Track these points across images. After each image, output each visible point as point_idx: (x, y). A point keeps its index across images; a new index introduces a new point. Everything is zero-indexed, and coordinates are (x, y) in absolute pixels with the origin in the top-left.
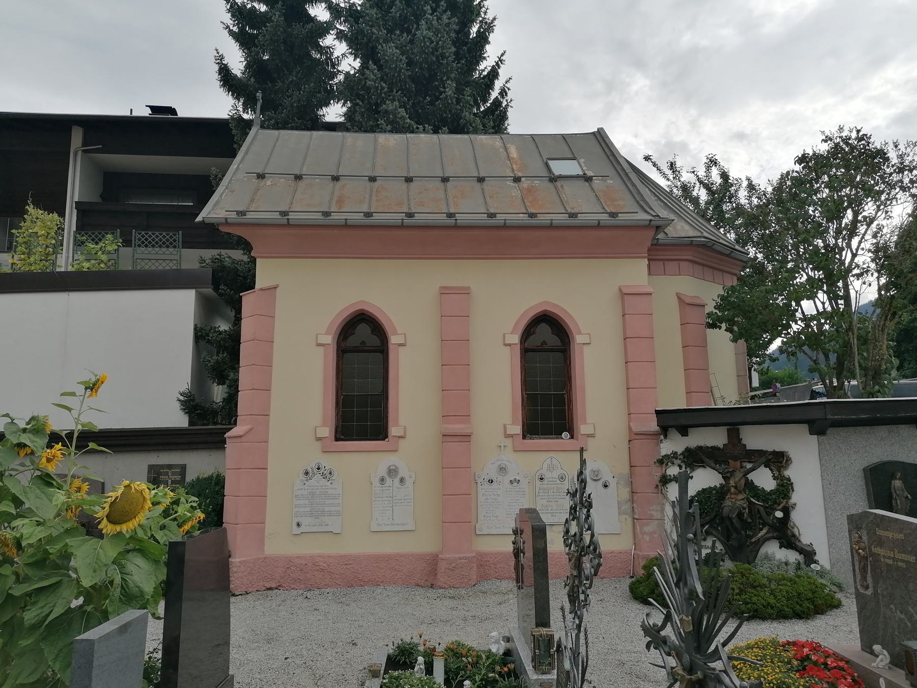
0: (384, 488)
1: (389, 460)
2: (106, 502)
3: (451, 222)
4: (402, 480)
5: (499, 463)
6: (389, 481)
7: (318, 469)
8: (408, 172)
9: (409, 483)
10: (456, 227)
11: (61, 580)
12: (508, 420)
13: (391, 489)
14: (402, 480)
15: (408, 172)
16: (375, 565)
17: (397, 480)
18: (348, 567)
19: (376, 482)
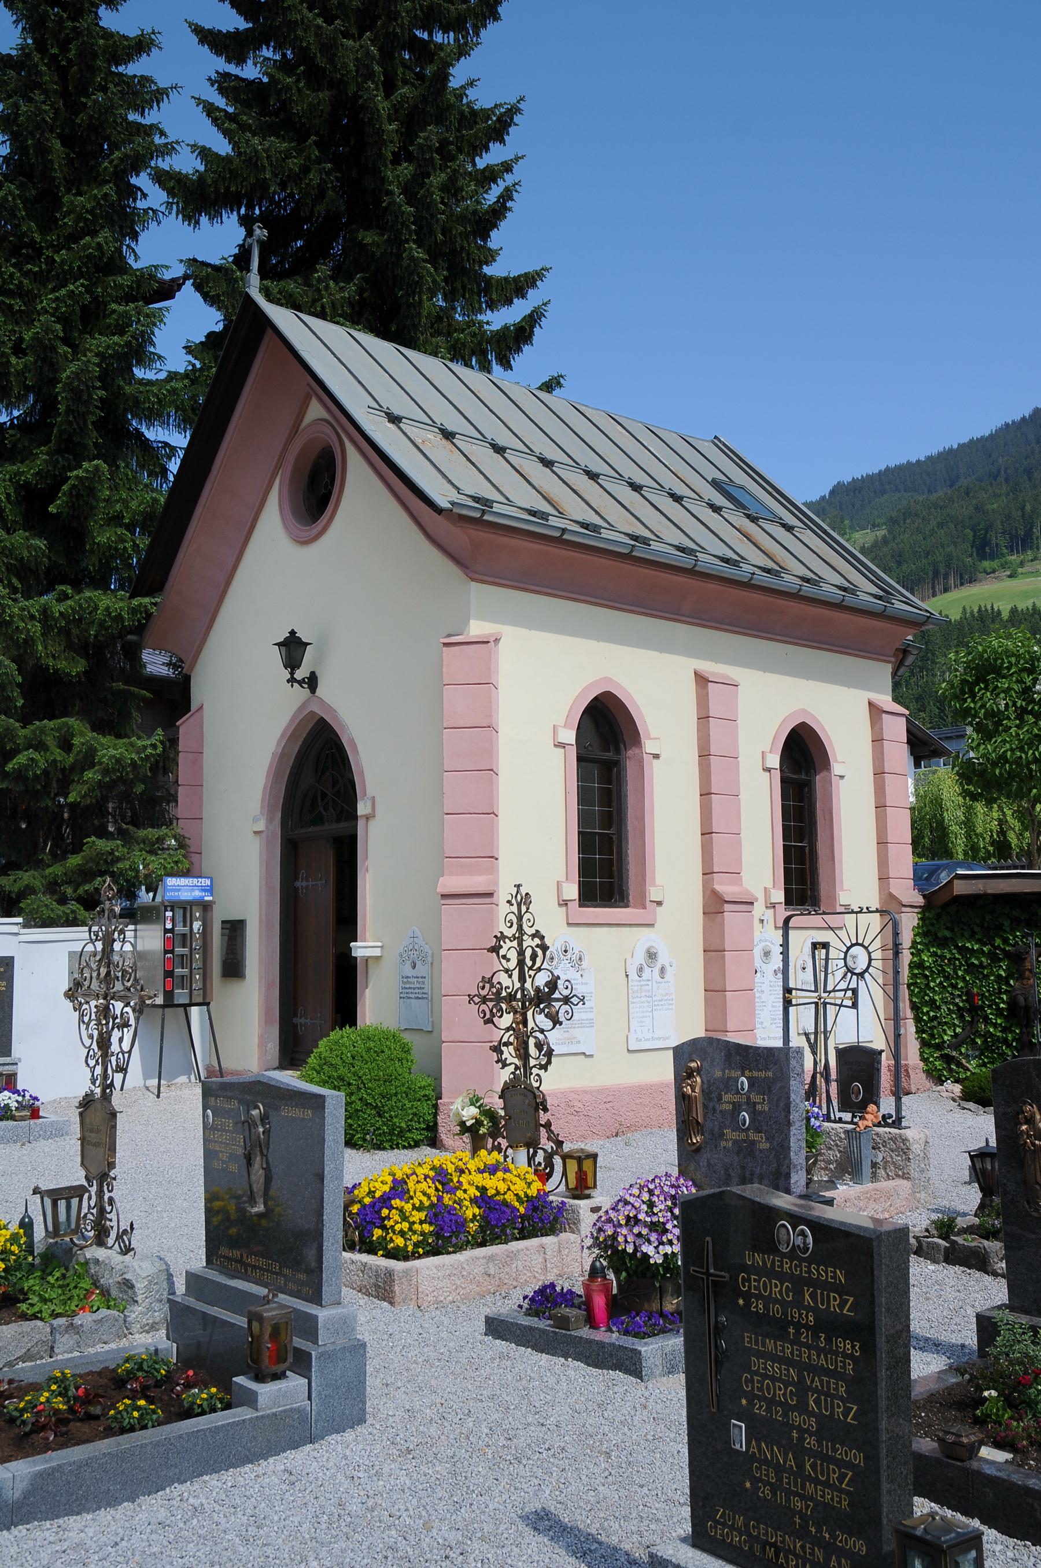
0: (643, 983)
1: (642, 939)
2: (826, 1360)
3: (687, 562)
4: (663, 970)
5: (763, 944)
6: (647, 971)
7: (566, 951)
8: (163, 1015)
9: (670, 973)
10: (692, 572)
11: (540, 388)
12: (769, 884)
13: (650, 983)
14: (663, 970)
15: (163, 1015)
16: (638, 1101)
17: (657, 970)
18: (608, 1106)
19: (633, 975)
